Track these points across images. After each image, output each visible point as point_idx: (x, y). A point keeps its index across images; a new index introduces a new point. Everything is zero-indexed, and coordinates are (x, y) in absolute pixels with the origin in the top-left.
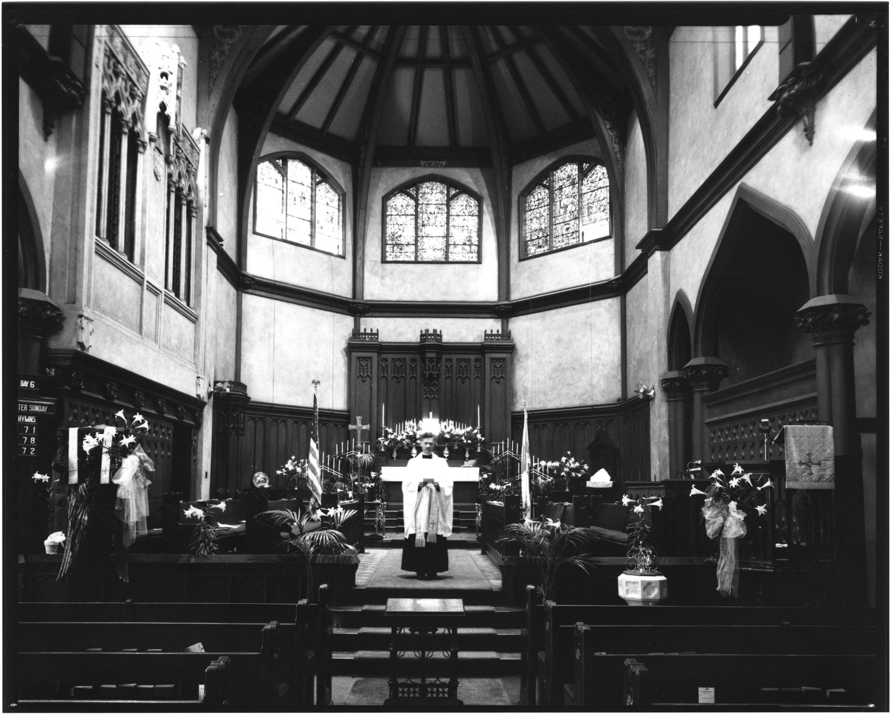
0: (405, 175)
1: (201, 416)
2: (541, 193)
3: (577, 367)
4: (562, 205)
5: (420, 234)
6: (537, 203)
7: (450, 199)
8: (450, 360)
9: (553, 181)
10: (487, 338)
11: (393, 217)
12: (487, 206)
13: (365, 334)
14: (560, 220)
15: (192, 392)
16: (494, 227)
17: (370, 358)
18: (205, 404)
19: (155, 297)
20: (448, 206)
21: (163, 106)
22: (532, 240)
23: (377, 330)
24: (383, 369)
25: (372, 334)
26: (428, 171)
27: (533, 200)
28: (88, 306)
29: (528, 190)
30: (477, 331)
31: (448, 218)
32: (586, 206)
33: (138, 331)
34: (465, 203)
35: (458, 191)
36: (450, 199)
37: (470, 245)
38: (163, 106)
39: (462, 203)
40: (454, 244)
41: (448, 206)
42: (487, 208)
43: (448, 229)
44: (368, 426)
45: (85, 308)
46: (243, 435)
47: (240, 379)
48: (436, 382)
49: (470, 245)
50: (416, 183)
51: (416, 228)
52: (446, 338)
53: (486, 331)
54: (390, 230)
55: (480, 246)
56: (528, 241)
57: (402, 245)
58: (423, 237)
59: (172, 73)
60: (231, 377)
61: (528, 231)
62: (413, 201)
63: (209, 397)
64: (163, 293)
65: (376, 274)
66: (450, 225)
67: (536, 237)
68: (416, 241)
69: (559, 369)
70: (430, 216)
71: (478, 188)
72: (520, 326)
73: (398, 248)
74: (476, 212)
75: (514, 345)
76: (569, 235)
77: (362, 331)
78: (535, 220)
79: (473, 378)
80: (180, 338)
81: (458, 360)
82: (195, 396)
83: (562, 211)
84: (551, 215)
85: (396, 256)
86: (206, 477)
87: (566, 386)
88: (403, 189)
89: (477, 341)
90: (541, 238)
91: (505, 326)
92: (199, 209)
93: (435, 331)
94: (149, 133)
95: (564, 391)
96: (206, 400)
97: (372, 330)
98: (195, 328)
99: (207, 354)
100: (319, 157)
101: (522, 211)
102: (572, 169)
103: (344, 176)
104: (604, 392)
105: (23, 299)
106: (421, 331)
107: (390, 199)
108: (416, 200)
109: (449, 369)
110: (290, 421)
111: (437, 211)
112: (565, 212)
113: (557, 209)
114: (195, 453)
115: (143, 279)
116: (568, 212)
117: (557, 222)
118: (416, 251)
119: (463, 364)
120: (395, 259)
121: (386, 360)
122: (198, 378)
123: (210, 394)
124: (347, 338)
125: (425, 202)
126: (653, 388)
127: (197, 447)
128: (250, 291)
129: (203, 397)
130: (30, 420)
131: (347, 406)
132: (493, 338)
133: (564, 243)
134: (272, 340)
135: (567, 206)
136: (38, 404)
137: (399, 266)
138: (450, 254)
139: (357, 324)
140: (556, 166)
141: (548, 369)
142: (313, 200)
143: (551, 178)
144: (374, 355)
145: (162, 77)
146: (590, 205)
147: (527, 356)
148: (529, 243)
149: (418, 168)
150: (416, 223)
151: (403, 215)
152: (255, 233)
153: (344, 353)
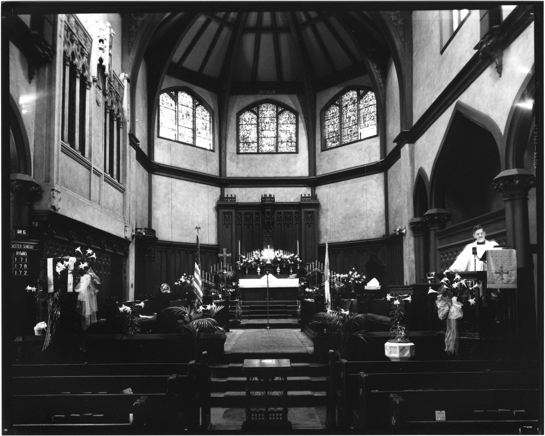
1: (128, 250)
2: (335, 109)
4: (347, 117)
6: (332, 115)
7: (278, 114)
9: (342, 102)
10: (302, 199)
12: (301, 118)
13: (228, 198)
14: (346, 125)
15: (122, 235)
16: (306, 131)
17: (231, 213)
20: (277, 118)
21: (101, 60)
22: (329, 138)
23: (235, 195)
25: (231, 198)
26: (264, 97)
27: (330, 113)
29: (327, 108)
32: (362, 117)
33: (89, 198)
34: (287, 116)
36: (278, 114)
37: (291, 142)
38: (101, 60)
41: (277, 118)
43: (277, 132)
49: (291, 142)
51: (258, 132)
52: (277, 200)
53: (301, 195)
54: (242, 133)
55: (297, 142)
56: (327, 139)
57: (249, 142)
58: (262, 138)
59: (106, 40)
60: (146, 226)
61: (327, 133)
62: (256, 116)
64: (103, 175)
67: (332, 136)
68: (258, 140)
70: (267, 125)
73: (247, 145)
74: (294, 121)
75: (319, 203)
76: (352, 135)
77: (226, 196)
81: (284, 213)
82: (124, 237)
83: (347, 120)
84: (341, 123)
85: (245, 149)
86: (132, 287)
88: (248, 109)
89: (296, 201)
91: (313, 192)
92: (124, 123)
93: (270, 195)
95: (350, 231)
96: (131, 240)
98: (123, 196)
100: (197, 89)
106: (262, 196)
107: (241, 114)
108: (257, 115)
110: (183, 252)
111: (270, 121)
112: (349, 121)
113: (345, 119)
116: (351, 120)
117: (345, 127)
118: (258, 146)
119: (288, 216)
120: (245, 152)
122: (126, 226)
123: (133, 236)
125: (263, 116)
126: (405, 228)
127: (126, 268)
129: (129, 238)
132: (306, 199)
133: (349, 140)
134: (170, 202)
136: (28, 244)
137: (248, 156)
138: (279, 148)
139: (222, 192)
140: (344, 92)
142: (194, 116)
143: (341, 100)
145: (100, 42)
147: (327, 210)
148: (327, 140)
150: (258, 129)
151: (250, 124)
152: (159, 137)
153: (215, 210)
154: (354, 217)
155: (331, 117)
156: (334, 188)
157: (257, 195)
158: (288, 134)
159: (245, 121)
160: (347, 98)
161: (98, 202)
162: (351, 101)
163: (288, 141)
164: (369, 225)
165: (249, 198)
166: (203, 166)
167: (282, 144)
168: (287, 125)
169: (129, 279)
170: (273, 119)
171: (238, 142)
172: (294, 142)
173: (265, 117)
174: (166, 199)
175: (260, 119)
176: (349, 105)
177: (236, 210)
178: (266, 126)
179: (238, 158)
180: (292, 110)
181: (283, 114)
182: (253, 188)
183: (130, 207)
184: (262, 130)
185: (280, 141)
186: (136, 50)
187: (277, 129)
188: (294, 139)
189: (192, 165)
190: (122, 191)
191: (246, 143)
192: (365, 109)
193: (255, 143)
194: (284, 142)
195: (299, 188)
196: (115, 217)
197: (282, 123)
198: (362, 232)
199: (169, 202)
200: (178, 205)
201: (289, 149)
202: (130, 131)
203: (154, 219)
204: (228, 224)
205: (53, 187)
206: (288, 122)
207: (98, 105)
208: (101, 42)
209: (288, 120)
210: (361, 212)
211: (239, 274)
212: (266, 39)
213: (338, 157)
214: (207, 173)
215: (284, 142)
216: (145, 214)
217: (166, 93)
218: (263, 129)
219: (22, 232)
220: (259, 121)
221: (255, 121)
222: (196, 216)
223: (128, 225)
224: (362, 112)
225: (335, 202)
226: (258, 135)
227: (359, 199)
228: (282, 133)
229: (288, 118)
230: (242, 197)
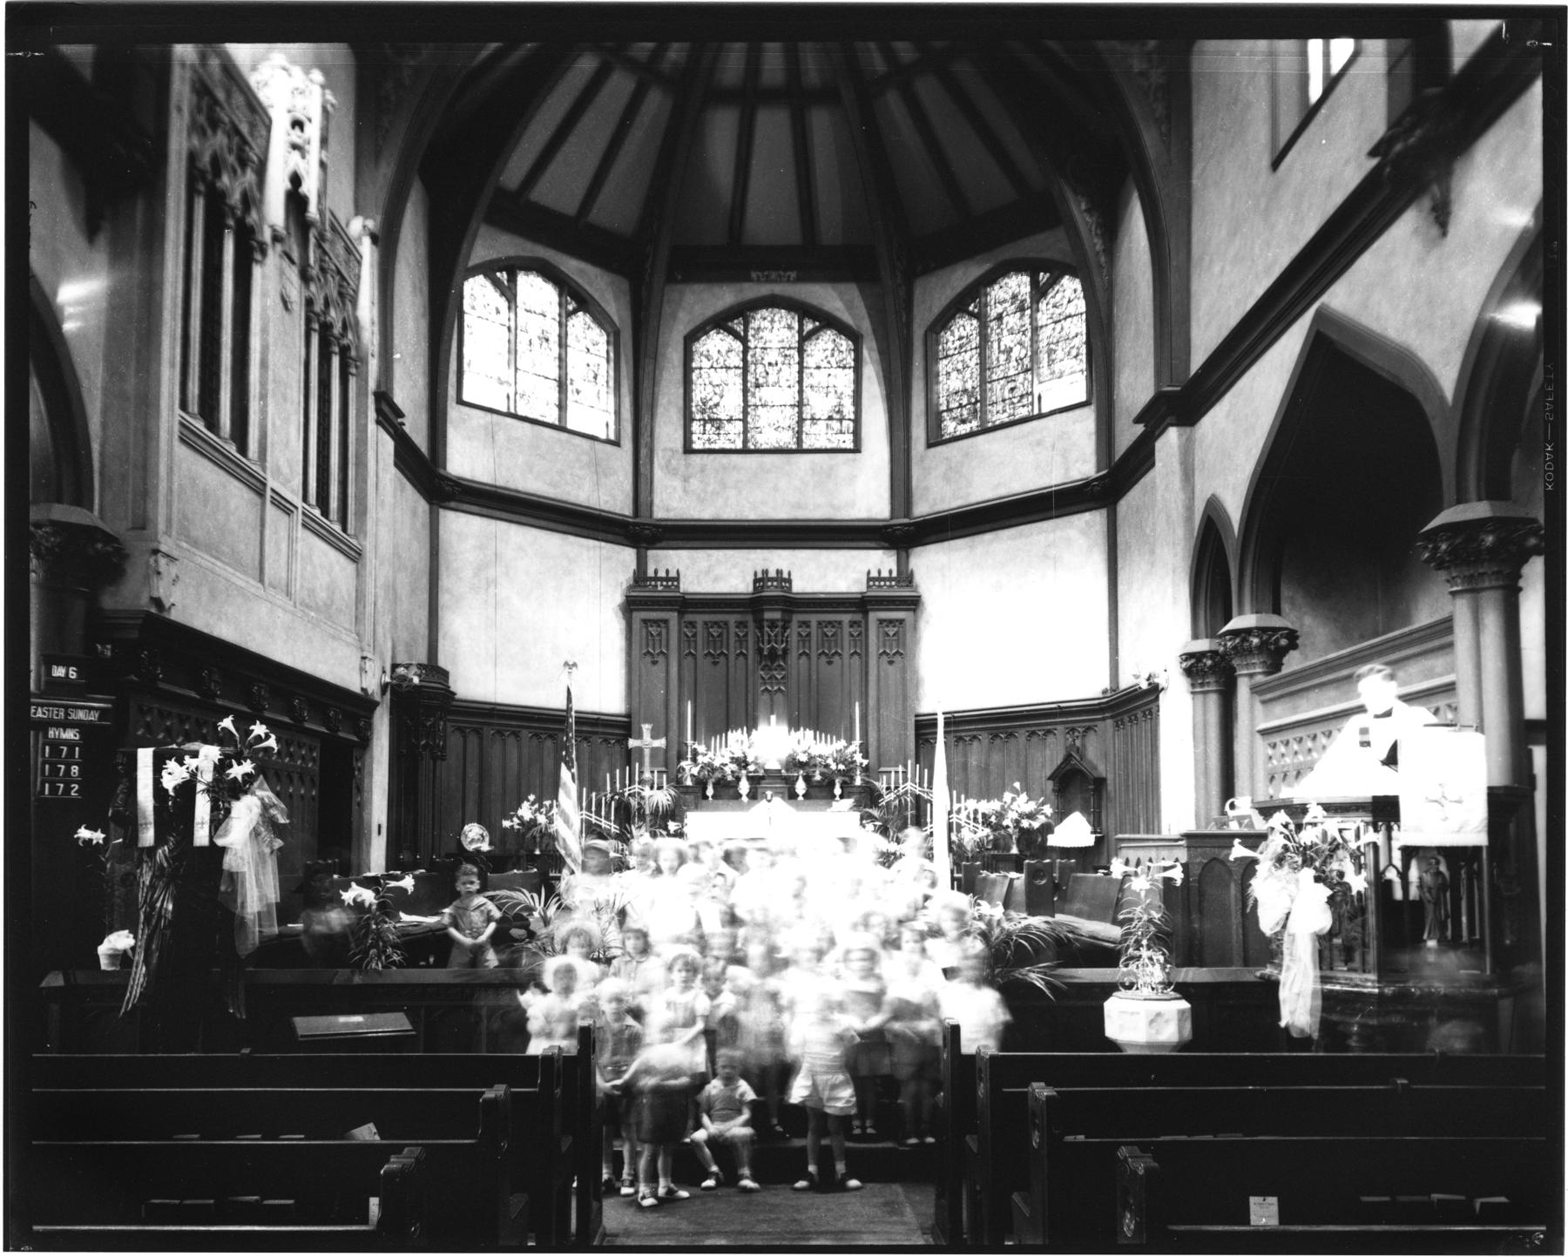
0: (725, 297)
2: (965, 327)
4: (1003, 348)
5: (752, 401)
7: (804, 338)
8: (806, 624)
10: (871, 583)
12: (870, 350)
13: (656, 579)
14: (999, 373)
16: (883, 387)
17: (666, 622)
18: (376, 704)
19: (286, 517)
20: (801, 351)
21: (296, 180)
22: (949, 410)
24: (687, 640)
25: (667, 579)
26: (764, 290)
27: (951, 338)
29: (943, 321)
31: (801, 372)
32: (1046, 349)
36: (804, 338)
37: (841, 420)
38: (296, 180)
39: (826, 346)
40: (813, 419)
41: (801, 351)
42: (869, 354)
43: (801, 392)
48: (782, 663)
49: (841, 420)
50: (744, 311)
51: (745, 391)
53: (869, 573)
54: (698, 395)
55: (857, 421)
56: (944, 411)
57: (720, 420)
58: (757, 406)
68: (745, 413)
70: (769, 369)
74: (850, 361)
75: (919, 597)
76: (1015, 400)
77: (651, 573)
79: (846, 655)
80: (331, 589)
81: (819, 623)
82: (357, 690)
83: (1003, 357)
84: (984, 366)
85: (709, 440)
86: (379, 833)
88: (719, 322)
91: (902, 563)
92: (362, 360)
93: (779, 572)
96: (377, 698)
97: (667, 572)
100: (571, 266)
101: (931, 359)
102: (1018, 284)
103: (616, 298)
106: (756, 574)
107: (698, 339)
108: (744, 340)
109: (805, 639)
110: (525, 734)
111: (780, 359)
112: (1008, 360)
113: (994, 354)
114: (360, 790)
115: (264, 485)
116: (1013, 359)
117: (994, 377)
118: (746, 431)
120: (707, 446)
121: (692, 624)
123: (384, 687)
125: (760, 345)
128: (453, 504)
130: (70, 735)
132: (882, 583)
133: (1006, 415)
136: (82, 708)
138: (804, 436)
139: (642, 563)
140: (991, 278)
142: (563, 343)
143: (983, 300)
144: (673, 617)
146: (1053, 346)
148: (945, 414)
150: (745, 381)
152: (460, 402)
159: (708, 358)
161: (285, 589)
166: (587, 485)
170: (787, 352)
171: (688, 419)
173: (765, 349)
176: (1007, 315)
177: (681, 613)
179: (687, 466)
183: (375, 604)
184: (758, 386)
185: (809, 417)
187: (800, 382)
189: (554, 485)
190: (355, 556)
202: (379, 385)
205: (154, 545)
209: (833, 355)
212: (772, 126)
223: (369, 655)
224: (1044, 335)
226: (745, 400)
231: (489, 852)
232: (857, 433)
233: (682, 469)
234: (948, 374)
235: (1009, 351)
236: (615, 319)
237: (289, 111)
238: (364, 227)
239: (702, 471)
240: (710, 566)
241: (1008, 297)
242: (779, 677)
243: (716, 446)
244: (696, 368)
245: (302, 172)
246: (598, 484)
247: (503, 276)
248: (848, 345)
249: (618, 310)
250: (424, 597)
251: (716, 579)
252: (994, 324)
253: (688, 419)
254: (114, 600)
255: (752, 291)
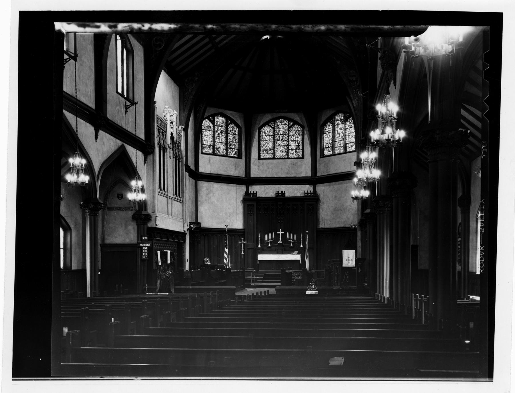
1: (185, 238)
3: (342, 210)
4: (338, 133)
6: (328, 130)
7: (289, 127)
9: (335, 121)
11: (263, 137)
12: (306, 131)
13: (251, 194)
16: (310, 141)
17: (253, 205)
18: (187, 233)
19: (171, 200)
20: (289, 131)
21: (172, 134)
22: (326, 148)
23: (256, 192)
25: (254, 194)
26: (279, 115)
27: (327, 128)
28: (157, 213)
29: (325, 124)
30: (302, 191)
31: (288, 136)
32: (348, 135)
34: (296, 129)
35: (293, 123)
36: (289, 127)
37: (299, 150)
38: (172, 134)
40: (291, 149)
42: (306, 132)
43: (288, 142)
44: (246, 242)
45: (157, 214)
46: (200, 243)
47: (198, 221)
48: (283, 215)
49: (299, 150)
50: (274, 120)
51: (274, 142)
52: (287, 195)
54: (262, 143)
55: (303, 150)
56: (325, 148)
57: (268, 150)
58: (277, 146)
59: (174, 121)
61: (325, 143)
62: (272, 129)
63: (188, 231)
65: (256, 165)
66: (290, 140)
67: (328, 147)
68: (274, 148)
69: (335, 210)
70: (281, 136)
71: (302, 122)
72: (322, 189)
73: (266, 152)
74: (301, 133)
76: (341, 147)
77: (250, 193)
78: (327, 138)
82: (183, 231)
83: (338, 135)
85: (265, 155)
86: (188, 261)
87: (338, 218)
88: (267, 124)
89: (302, 196)
90: (329, 147)
92: (182, 158)
93: (282, 192)
94: (168, 145)
95: (338, 220)
96: (187, 232)
97: (254, 192)
98: (182, 205)
99: (186, 214)
100: (228, 113)
103: (240, 119)
104: (352, 221)
105: (143, 214)
106: (276, 192)
107: (262, 128)
111: (283, 133)
112: (339, 136)
114: (184, 252)
115: (168, 196)
116: (340, 136)
117: (336, 140)
118: (274, 153)
120: (264, 157)
123: (188, 229)
124: (243, 196)
125: (278, 129)
127: (184, 250)
128: (200, 179)
130: (146, 248)
131: (244, 227)
133: (339, 151)
134: (210, 200)
135: (340, 133)
136: (147, 244)
137: (266, 161)
138: (289, 154)
141: (331, 209)
143: (334, 119)
145: (171, 124)
146: (349, 134)
147: (323, 203)
148: (325, 149)
149: (274, 114)
150: (274, 139)
151: (268, 136)
152: (202, 153)
153: (242, 203)
154: (340, 210)
155: (328, 131)
156: (328, 187)
157: (273, 191)
158: (297, 143)
159: (265, 133)
160: (338, 119)
162: (340, 121)
163: (296, 149)
164: (349, 216)
165: (267, 193)
166: (233, 170)
167: (292, 151)
168: (295, 136)
169: (186, 256)
170: (285, 131)
171: (259, 150)
172: (301, 149)
173: (279, 130)
174: (207, 198)
175: (276, 131)
176: (339, 124)
178: (280, 137)
179: (259, 163)
180: (300, 125)
181: (293, 127)
182: (270, 186)
184: (277, 140)
185: (291, 149)
186: (188, 109)
187: (288, 139)
188: (301, 147)
189: (225, 171)
190: (182, 202)
191: (266, 150)
192: (349, 129)
193: (272, 151)
194: (293, 149)
195: (304, 186)
196: (178, 220)
197: (292, 135)
198: (345, 222)
199: (209, 200)
200: (216, 201)
201: (297, 154)
202: (185, 163)
203: (199, 213)
204: (252, 213)
205: (156, 216)
206: (297, 133)
207: (170, 159)
208: (172, 124)
209: (297, 132)
210: (345, 207)
211: (259, 250)
213: (331, 164)
214: (236, 176)
215: (293, 149)
216: (194, 210)
217: (206, 119)
218: (278, 139)
219: (145, 238)
220: (275, 133)
221: (272, 133)
222: (228, 208)
223: (185, 223)
224: (348, 130)
225: (328, 197)
226: (274, 144)
227: (343, 197)
228: (292, 142)
229: (297, 130)
230: (262, 193)
231: (210, 264)
232: (303, 155)
233: (258, 164)
234: (326, 138)
235: (339, 134)
236: (240, 125)
237: (170, 121)
238: (182, 128)
239: (263, 164)
240: (265, 190)
241: (339, 119)
242: (282, 219)
243: (267, 157)
244: (261, 136)
245: (173, 132)
246: (236, 170)
247: (211, 118)
248: (301, 129)
249: (241, 122)
250: (194, 204)
251: (267, 193)
252: (336, 126)
253: (259, 150)
254: (150, 225)
255: (275, 115)
